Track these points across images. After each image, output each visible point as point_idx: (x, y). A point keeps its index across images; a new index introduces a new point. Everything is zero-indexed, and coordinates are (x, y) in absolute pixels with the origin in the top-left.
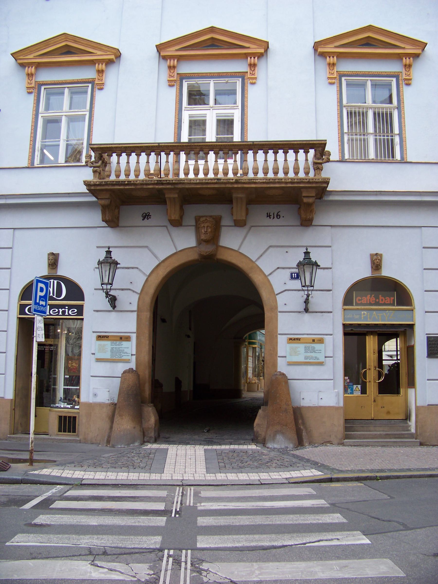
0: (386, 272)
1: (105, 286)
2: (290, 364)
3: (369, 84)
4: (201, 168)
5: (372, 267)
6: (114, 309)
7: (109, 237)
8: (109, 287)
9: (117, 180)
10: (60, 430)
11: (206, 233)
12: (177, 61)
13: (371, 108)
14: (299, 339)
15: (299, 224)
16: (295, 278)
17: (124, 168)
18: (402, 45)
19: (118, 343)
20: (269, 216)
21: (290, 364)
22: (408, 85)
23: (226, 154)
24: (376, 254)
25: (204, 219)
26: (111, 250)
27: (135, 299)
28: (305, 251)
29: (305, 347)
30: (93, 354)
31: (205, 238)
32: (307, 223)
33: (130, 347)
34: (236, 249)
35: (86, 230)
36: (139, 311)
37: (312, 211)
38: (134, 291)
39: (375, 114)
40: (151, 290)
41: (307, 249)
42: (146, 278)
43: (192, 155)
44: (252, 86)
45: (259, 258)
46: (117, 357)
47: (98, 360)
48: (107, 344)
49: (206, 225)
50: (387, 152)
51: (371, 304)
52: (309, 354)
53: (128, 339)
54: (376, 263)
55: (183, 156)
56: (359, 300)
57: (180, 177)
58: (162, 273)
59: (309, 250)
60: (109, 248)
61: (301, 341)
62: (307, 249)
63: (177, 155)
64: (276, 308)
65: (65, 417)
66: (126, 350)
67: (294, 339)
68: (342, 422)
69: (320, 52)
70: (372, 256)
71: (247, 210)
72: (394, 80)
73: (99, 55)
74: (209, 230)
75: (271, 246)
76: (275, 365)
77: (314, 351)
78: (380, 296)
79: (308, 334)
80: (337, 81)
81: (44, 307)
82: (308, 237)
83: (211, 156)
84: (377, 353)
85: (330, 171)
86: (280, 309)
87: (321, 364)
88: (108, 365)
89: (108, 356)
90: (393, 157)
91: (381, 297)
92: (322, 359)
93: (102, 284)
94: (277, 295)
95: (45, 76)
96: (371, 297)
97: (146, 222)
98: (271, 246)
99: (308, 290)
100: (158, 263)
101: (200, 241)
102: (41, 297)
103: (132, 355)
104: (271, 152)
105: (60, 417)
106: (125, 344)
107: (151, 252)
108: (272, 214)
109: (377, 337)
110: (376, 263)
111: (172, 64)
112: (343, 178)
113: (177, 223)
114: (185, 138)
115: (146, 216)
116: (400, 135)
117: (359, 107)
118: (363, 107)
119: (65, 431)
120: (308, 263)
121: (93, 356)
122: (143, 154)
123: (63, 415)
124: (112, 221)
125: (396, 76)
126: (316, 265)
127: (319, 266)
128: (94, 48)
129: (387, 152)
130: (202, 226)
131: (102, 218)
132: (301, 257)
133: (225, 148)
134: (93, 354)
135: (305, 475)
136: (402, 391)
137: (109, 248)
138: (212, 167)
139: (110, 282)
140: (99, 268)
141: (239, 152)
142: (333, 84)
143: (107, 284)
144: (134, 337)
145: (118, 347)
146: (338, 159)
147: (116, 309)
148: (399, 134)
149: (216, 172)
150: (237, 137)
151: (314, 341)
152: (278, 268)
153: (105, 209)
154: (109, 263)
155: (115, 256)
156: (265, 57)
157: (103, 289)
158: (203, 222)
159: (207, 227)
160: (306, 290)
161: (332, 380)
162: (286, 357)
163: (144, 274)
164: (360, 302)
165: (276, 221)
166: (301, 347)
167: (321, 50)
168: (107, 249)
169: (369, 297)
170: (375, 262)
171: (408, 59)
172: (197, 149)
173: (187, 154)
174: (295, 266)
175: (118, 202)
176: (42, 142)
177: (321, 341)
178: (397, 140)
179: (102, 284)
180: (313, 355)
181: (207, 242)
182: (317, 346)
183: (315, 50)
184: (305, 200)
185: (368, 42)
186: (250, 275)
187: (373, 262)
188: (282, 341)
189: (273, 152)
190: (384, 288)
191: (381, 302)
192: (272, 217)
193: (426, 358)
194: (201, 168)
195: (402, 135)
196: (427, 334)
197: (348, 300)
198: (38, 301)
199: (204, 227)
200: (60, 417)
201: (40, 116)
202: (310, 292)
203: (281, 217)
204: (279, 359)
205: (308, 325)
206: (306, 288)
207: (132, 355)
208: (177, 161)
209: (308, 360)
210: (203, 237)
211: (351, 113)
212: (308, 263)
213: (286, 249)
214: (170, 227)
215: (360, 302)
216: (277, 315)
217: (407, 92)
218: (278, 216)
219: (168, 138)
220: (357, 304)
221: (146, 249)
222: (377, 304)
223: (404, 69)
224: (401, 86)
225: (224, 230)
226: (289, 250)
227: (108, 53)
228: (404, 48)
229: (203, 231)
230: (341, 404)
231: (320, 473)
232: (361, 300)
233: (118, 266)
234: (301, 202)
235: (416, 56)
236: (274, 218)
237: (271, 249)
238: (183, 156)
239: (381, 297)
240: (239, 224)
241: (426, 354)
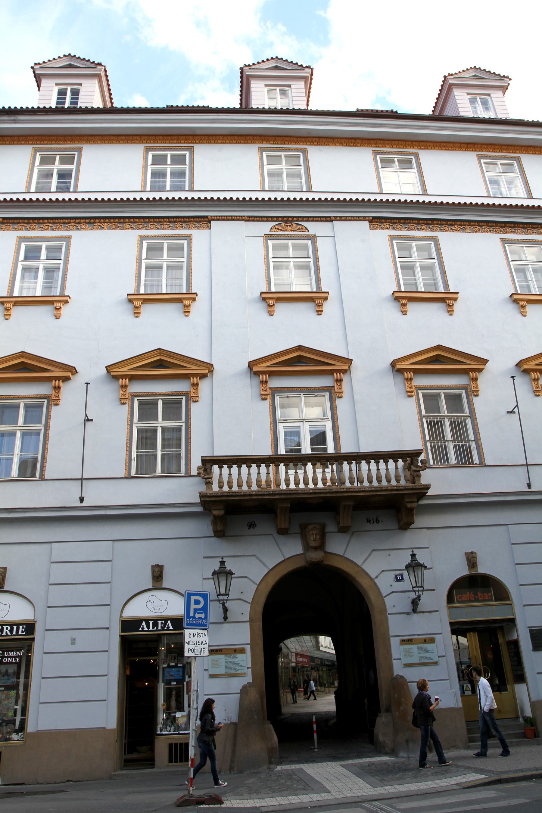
0: (481, 569)
1: (221, 598)
2: (406, 665)
3: (160, 403)
4: (301, 477)
5: (468, 565)
6: (225, 620)
7: (223, 548)
8: (225, 597)
9: (278, 489)
10: (170, 761)
11: (315, 540)
12: (129, 380)
13: (447, 417)
14: (411, 640)
15: (398, 528)
16: (400, 580)
17: (226, 480)
18: (469, 362)
19: (232, 656)
20: (369, 521)
21: (406, 665)
22: (477, 396)
23: (296, 465)
24: (472, 553)
25: (312, 526)
26: (224, 560)
27: (247, 608)
28: (411, 553)
29: (418, 648)
30: (205, 670)
31: (315, 545)
32: (405, 525)
33: (245, 660)
34: (342, 554)
35: (190, 540)
36: (252, 621)
37: (412, 516)
38: (244, 601)
39: (451, 422)
40: (262, 600)
41: (413, 551)
42: (256, 587)
43: (318, 464)
44: (340, 399)
45: (364, 562)
46: (232, 672)
47: (212, 676)
48: (221, 658)
49: (315, 532)
50: (465, 457)
51: (471, 601)
52: (422, 655)
53: (242, 651)
54: (471, 560)
55: (282, 467)
56: (460, 598)
57: (213, 490)
58: (272, 581)
59: (414, 553)
60: (222, 559)
61: (414, 641)
62: (413, 551)
63: (277, 466)
64: (385, 610)
65: (176, 745)
66: (241, 663)
67: (407, 641)
68: (464, 724)
69: (398, 368)
70: (466, 554)
71: (290, 518)
72: (464, 391)
73: (193, 369)
74: (318, 537)
75: (373, 550)
76: (390, 668)
77: (426, 651)
78: (479, 592)
79: (419, 635)
80: (269, 398)
81: (203, 619)
82: (410, 539)
83: (309, 466)
84: (492, 649)
85: (427, 477)
86: (389, 611)
87: (435, 663)
88: (224, 681)
89: (222, 670)
90: (472, 461)
91: (480, 594)
92: (436, 659)
93: (218, 595)
94: (385, 597)
95: (275, 383)
96: (470, 594)
97: (252, 531)
98: (373, 550)
99: (418, 591)
100: (266, 571)
101: (307, 547)
102: (195, 610)
103: (248, 668)
104: (225, 466)
105: (170, 745)
106: (240, 657)
107: (260, 562)
108: (371, 519)
109: (476, 633)
110: (471, 560)
111: (124, 384)
112: (440, 481)
113: (283, 532)
114: (282, 451)
115: (252, 525)
116: (477, 440)
117: (437, 417)
118: (440, 417)
119: (176, 761)
120: (414, 566)
121: (206, 672)
122: (235, 466)
123: (173, 742)
124: (220, 533)
125: (465, 387)
126: (423, 566)
127: (426, 567)
128: (188, 363)
129: (465, 457)
130: (311, 533)
131: (213, 529)
132: (409, 560)
133: (321, 459)
134: (205, 670)
135: (282, 802)
136: (509, 687)
137: (222, 559)
138: (314, 478)
139: (227, 593)
140: (213, 578)
141: (271, 464)
142: (412, 396)
143: (223, 595)
144: (248, 648)
145: (232, 660)
146: (123, 476)
147: (227, 620)
148: (474, 440)
149: (324, 481)
150: (331, 449)
151: (425, 641)
152: (383, 571)
153: (216, 521)
154: (223, 573)
155: (229, 566)
156: (348, 372)
157: (219, 600)
158: (312, 530)
159: (316, 534)
160: (417, 591)
161: (447, 680)
162: (401, 659)
163: (254, 583)
164: (461, 599)
165: (376, 526)
166: (414, 648)
167: (397, 368)
168: (220, 560)
169: (468, 594)
170: (472, 560)
171: (195, 378)
172: (295, 459)
173: (286, 466)
174: (404, 568)
175: (230, 514)
176: (137, 452)
177: (432, 641)
178: (473, 445)
179: (218, 595)
180: (427, 655)
181: (316, 548)
182: (429, 646)
183: (392, 366)
184: (409, 505)
185: (436, 359)
186: (358, 579)
187: (468, 560)
188: (395, 643)
189: (256, 466)
190: (476, 584)
191: (480, 598)
192: (372, 522)
193: (532, 652)
194: (301, 477)
195: (478, 441)
196: (528, 627)
197: (450, 599)
198: (192, 614)
199: (313, 534)
200: (170, 745)
201: (134, 426)
202: (420, 593)
203: (380, 521)
204: (394, 661)
205: (419, 625)
206: (417, 589)
207: (248, 668)
208: (277, 472)
209: (422, 661)
210: (313, 544)
211: (430, 422)
212: (414, 566)
213: (388, 552)
214: (276, 535)
215: (461, 599)
216: (387, 617)
217: (476, 401)
218: (377, 521)
219: (267, 451)
220: (459, 602)
221: (254, 558)
222: (477, 600)
223: (336, 384)
224: (470, 397)
225: (328, 535)
226: (392, 552)
227: (203, 368)
228: (469, 364)
229: (312, 538)
230: (460, 705)
231: (483, 776)
232: (461, 598)
233: (233, 576)
234: (396, 507)
235: (480, 370)
236: (373, 523)
237: (374, 553)
238: (282, 467)
239: (480, 594)
240: (343, 530)
241: (531, 648)
